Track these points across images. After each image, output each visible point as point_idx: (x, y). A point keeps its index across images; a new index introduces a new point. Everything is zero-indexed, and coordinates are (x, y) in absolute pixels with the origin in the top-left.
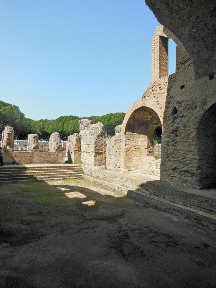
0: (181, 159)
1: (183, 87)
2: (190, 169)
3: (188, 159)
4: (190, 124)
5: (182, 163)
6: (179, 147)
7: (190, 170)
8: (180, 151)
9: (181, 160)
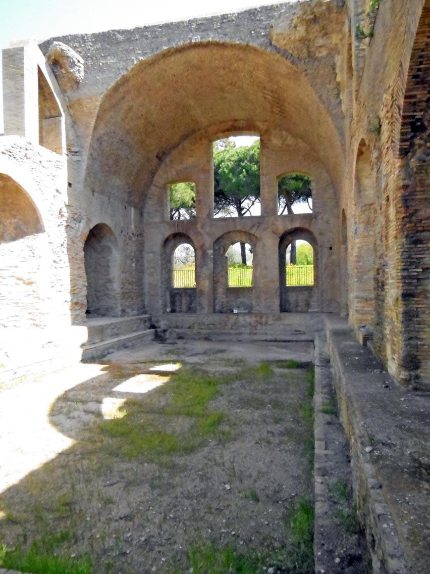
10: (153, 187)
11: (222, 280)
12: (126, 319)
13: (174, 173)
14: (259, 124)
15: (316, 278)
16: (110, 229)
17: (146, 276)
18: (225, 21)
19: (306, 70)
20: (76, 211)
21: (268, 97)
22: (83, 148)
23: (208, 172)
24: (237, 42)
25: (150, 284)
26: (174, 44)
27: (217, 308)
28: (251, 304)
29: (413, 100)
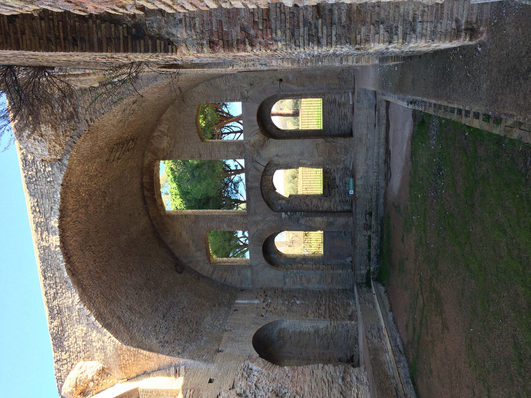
10: (214, 277)
12: (359, 313)
13: (198, 254)
14: (146, 162)
15: (314, 95)
17: (310, 287)
18: (38, 210)
19: (87, 121)
20: (240, 375)
21: (117, 155)
22: (171, 363)
23: (197, 217)
25: (319, 283)
26: (62, 264)
27: (347, 208)
28: (342, 169)
29: (104, 41)
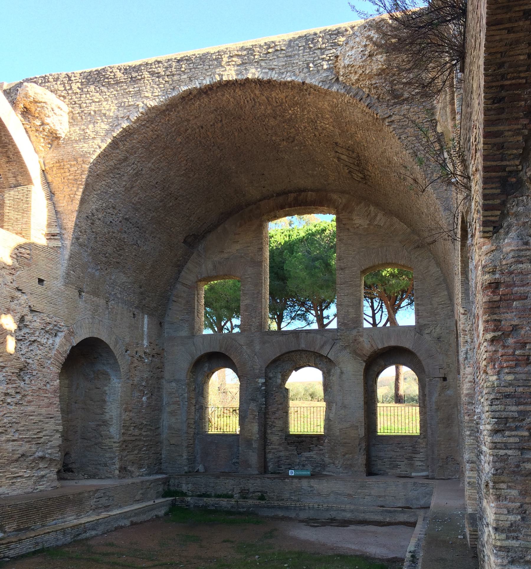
0: (35, 434)
1: (41, 281)
2: (49, 451)
3: (47, 432)
4: (49, 362)
5: (35, 443)
6: (30, 408)
7: (50, 454)
8: (32, 416)
9: (35, 436)
10: (179, 286)
11: (279, 423)
13: (210, 266)
14: (335, 196)
16: (107, 346)
20: (48, 320)
21: (343, 157)
22: (65, 229)
23: (260, 264)
24: (289, 79)
25: (170, 428)
26: (197, 83)
